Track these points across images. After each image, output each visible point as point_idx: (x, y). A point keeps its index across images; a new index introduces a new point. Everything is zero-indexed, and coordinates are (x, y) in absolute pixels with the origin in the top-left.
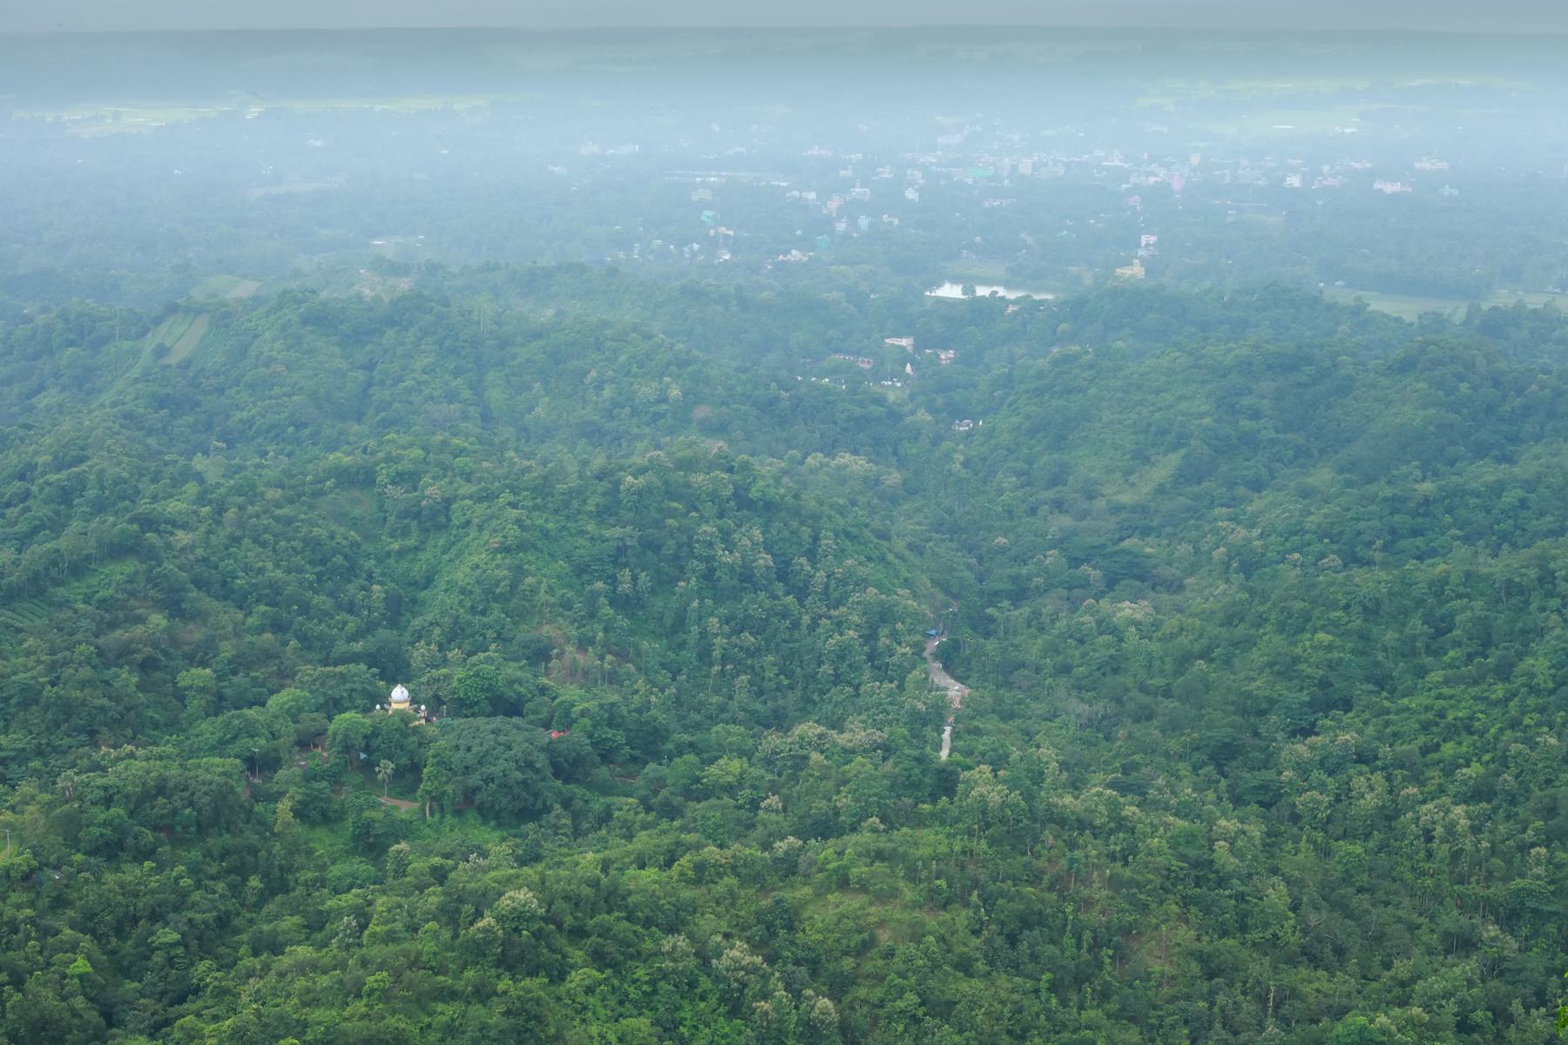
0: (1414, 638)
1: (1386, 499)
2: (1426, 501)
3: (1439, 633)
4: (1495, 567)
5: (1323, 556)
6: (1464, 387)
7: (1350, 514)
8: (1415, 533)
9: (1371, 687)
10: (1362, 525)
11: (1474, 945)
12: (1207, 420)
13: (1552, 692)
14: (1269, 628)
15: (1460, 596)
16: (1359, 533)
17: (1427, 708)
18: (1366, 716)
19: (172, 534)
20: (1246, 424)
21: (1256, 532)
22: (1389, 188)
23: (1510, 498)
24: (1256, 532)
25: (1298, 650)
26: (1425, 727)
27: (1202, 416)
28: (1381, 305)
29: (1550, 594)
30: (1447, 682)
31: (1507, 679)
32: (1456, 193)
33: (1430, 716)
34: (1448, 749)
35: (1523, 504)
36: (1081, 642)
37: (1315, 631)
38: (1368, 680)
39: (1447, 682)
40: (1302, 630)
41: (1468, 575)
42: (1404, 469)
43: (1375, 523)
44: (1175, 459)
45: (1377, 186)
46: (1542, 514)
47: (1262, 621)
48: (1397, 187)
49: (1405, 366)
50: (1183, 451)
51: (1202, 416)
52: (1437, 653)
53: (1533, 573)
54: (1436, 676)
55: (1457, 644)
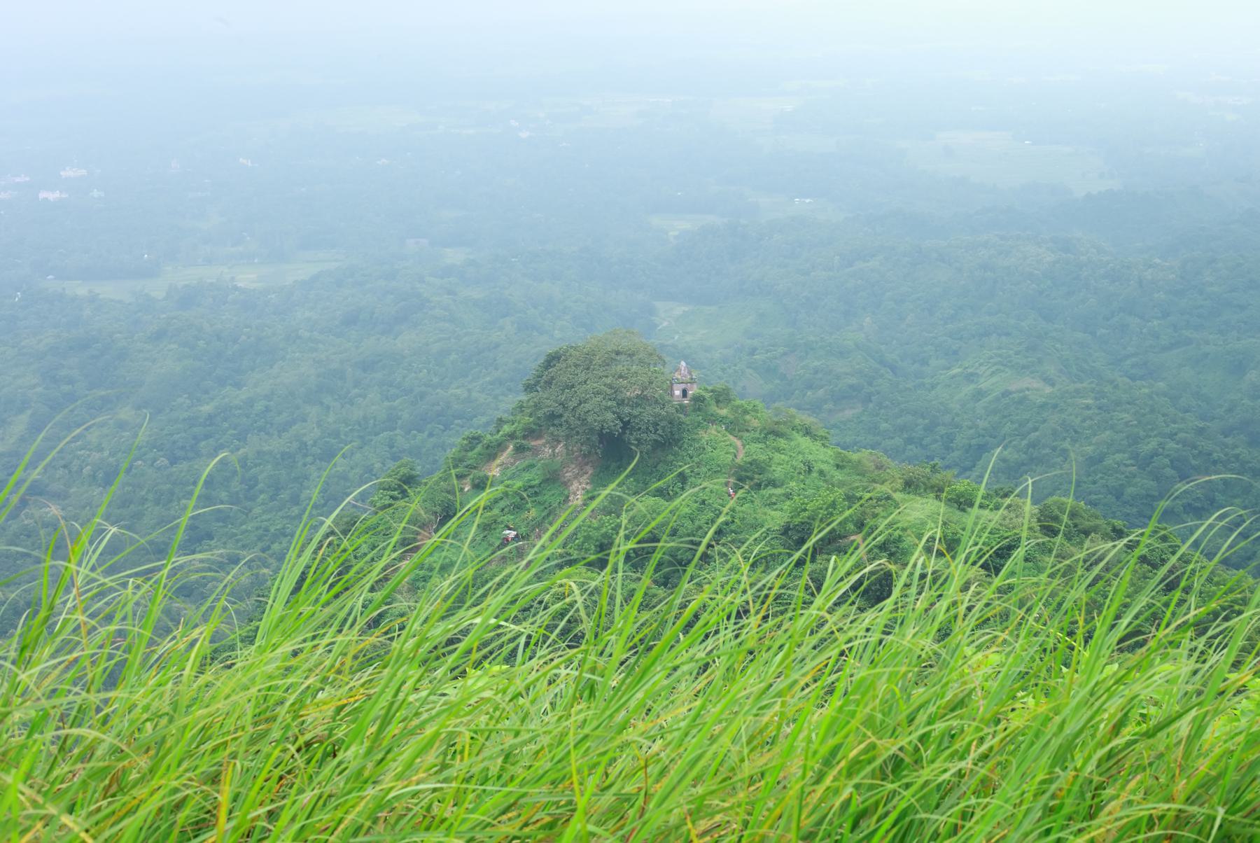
0: (237, 493)
1: (184, 420)
2: (210, 418)
3: (251, 487)
4: (276, 444)
5: (155, 460)
6: (201, 343)
8: (207, 437)
10: (176, 437)
11: (601, 435)
12: (39, 389)
15: (256, 465)
16: (174, 442)
17: (257, 529)
18: (224, 539)
20: (66, 388)
21: (106, 453)
22: (53, 196)
23: (259, 406)
24: (106, 453)
25: (172, 512)
26: (260, 539)
27: (34, 386)
28: (107, 290)
29: (305, 455)
30: (264, 512)
31: (297, 504)
33: (261, 532)
34: (276, 547)
35: (267, 409)
36: (29, 536)
37: (179, 500)
38: (218, 520)
39: (264, 512)
40: (171, 501)
41: (258, 453)
42: (180, 400)
43: (183, 435)
44: (24, 418)
45: (42, 195)
47: (144, 500)
48: (57, 195)
49: (159, 336)
50: (29, 412)
51: (34, 386)
52: (253, 499)
53: (295, 445)
54: (257, 510)
55: (261, 492)
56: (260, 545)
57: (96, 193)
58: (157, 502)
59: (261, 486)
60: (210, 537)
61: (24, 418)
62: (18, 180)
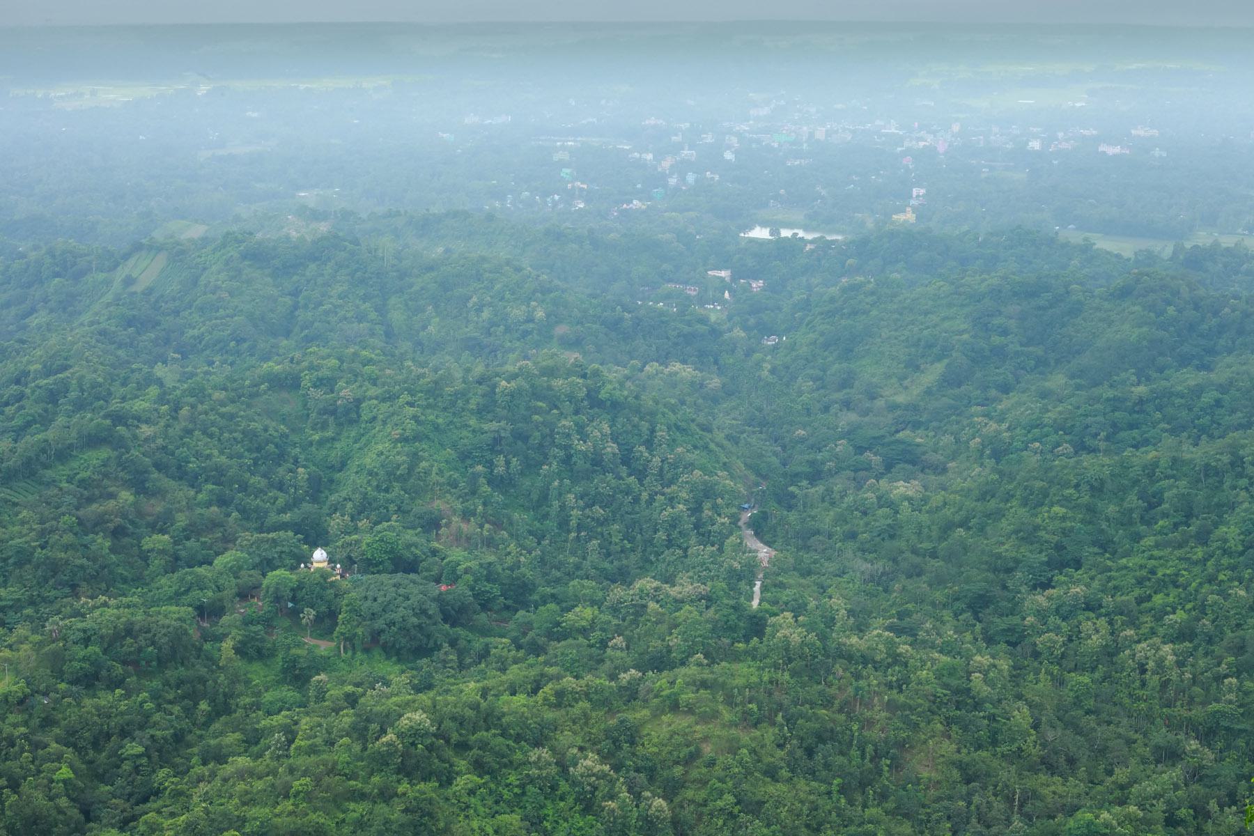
0: (1131, 510)
1: (1108, 400)
2: (1141, 401)
3: (1151, 506)
4: (1196, 454)
6: (1171, 310)
7: (1080, 412)
8: (1132, 426)
9: (1096, 550)
10: (1090, 420)
12: (965, 336)
13: (1242, 554)
15: (1167, 477)
16: (1087, 427)
17: (1141, 567)
18: (1093, 572)
20: (997, 340)
21: (1004, 426)
22: (1113, 150)
23: (1207, 399)
24: (1004, 426)
25: (1039, 520)
26: (1140, 582)
27: (961, 332)
29: (1240, 475)
30: (1157, 546)
32: (1164, 154)
34: (1158, 599)
35: (1218, 403)
36: (865, 513)
38: (1094, 544)
39: (1157, 546)
40: (1042, 504)
42: (1123, 375)
43: (1100, 419)
44: (940, 367)
45: (1101, 149)
46: (1233, 411)
47: (1009, 497)
49: (1124, 293)
50: (946, 361)
51: (961, 332)
52: (1149, 523)
53: (1226, 459)
54: (1148, 541)
55: (1165, 515)
56: (1137, 592)
57: (1157, 152)
58: (1025, 503)
59: (1165, 506)
60: (1078, 564)
61: (940, 367)
62: (1086, 132)
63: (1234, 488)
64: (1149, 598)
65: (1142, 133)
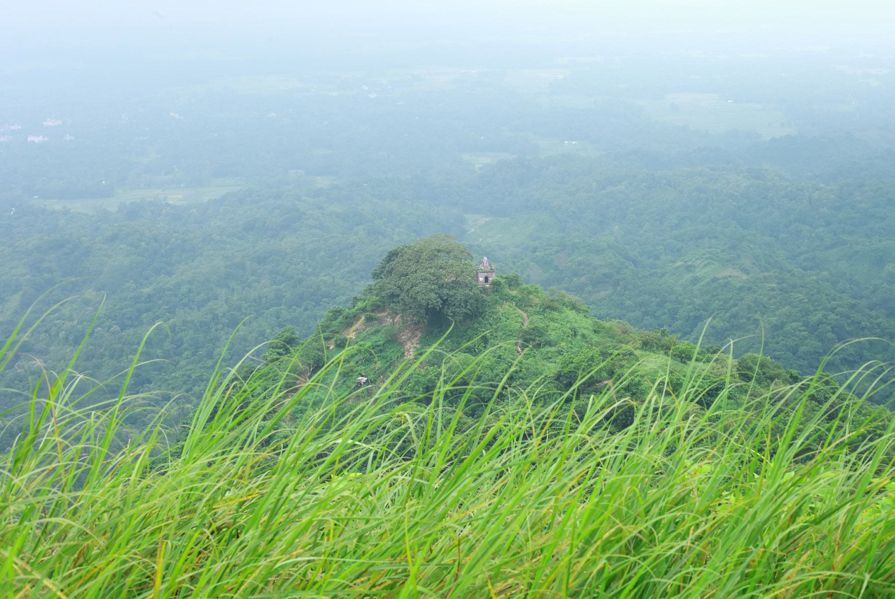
1: (131, 298)
2: (149, 296)
4: (195, 316)
5: (110, 327)
6: (143, 244)
7: (117, 307)
9: (157, 372)
13: (231, 358)
14: (105, 358)
16: (124, 314)
17: (183, 375)
18: (159, 384)
19: (779, 283)
20: (47, 276)
21: (75, 322)
22: (38, 139)
23: (184, 289)
26: (185, 383)
29: (217, 324)
32: (73, 138)
33: (185, 378)
34: (196, 389)
35: (190, 291)
36: (21, 381)
38: (155, 370)
39: (188, 364)
44: (17, 297)
45: (30, 139)
46: (199, 293)
48: (41, 138)
49: (113, 239)
50: (21, 293)
52: (180, 354)
53: (210, 316)
54: (183, 363)
55: (186, 349)
56: (185, 387)
59: (185, 345)
60: (150, 382)
61: (17, 297)
63: (216, 330)
64: (191, 389)
65: (51, 124)
